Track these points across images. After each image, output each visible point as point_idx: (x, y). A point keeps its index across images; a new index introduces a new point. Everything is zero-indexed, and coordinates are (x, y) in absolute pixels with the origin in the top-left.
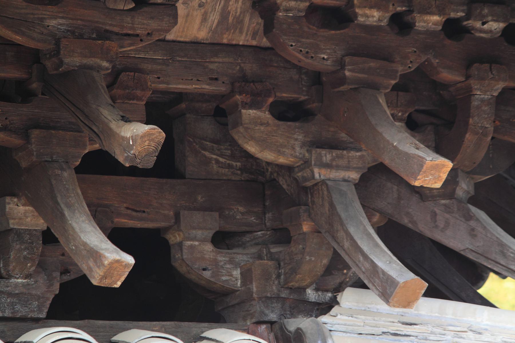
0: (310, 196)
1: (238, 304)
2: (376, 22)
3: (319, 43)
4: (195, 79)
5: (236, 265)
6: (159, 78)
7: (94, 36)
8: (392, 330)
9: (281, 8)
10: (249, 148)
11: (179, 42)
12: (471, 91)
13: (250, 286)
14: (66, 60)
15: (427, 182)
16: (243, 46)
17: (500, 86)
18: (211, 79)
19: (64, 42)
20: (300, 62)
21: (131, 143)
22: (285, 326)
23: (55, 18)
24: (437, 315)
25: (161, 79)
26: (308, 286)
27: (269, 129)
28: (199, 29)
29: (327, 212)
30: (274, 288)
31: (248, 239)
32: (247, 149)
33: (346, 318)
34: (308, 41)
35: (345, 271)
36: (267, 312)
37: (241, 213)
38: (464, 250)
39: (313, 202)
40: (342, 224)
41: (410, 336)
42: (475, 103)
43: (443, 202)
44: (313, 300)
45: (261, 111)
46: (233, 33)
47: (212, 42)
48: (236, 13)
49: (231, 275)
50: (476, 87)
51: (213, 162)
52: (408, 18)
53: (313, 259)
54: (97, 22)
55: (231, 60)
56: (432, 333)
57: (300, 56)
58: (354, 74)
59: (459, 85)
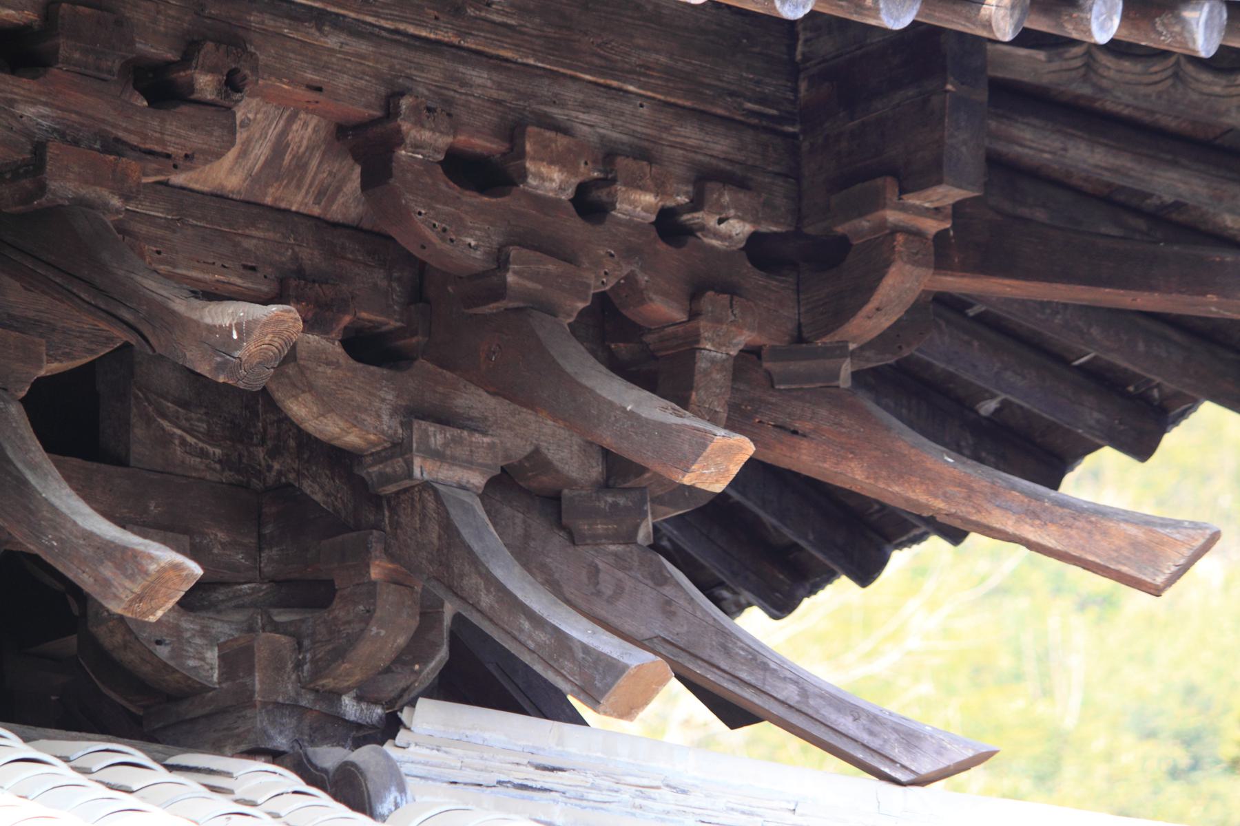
0: (387, 513)
1: (207, 716)
2: (555, 190)
3: (463, 215)
4: (218, 263)
5: (212, 641)
6: (159, 253)
7: (97, 146)
8: (518, 776)
9: (408, 141)
10: (295, 408)
11: (192, 190)
12: (698, 342)
13: (248, 681)
14: (53, 185)
15: (704, 478)
16: (297, 213)
17: (745, 338)
18: (245, 267)
19: (52, 150)
20: (423, 247)
21: (235, 337)
22: (309, 760)
23: (34, 103)
24: (599, 754)
25: (164, 255)
26: (347, 690)
27: (340, 373)
28: (231, 171)
29: (436, 541)
30: (288, 688)
31: (221, 598)
32: (291, 409)
33: (427, 751)
34: (447, 209)
35: (417, 667)
36: (272, 732)
37: (221, 544)
38: (650, 639)
39: (396, 525)
40: (474, 561)
41: (550, 791)
42: (702, 365)
43: (612, 548)
44: (352, 718)
45: (327, 340)
46: (286, 186)
47: (247, 199)
48: (299, 147)
49: (203, 659)
50: (706, 334)
51: (177, 442)
52: (602, 195)
53: (383, 633)
54: (103, 121)
55: (278, 236)
56: (594, 787)
57: (429, 233)
58: (521, 281)
59: (670, 330)
